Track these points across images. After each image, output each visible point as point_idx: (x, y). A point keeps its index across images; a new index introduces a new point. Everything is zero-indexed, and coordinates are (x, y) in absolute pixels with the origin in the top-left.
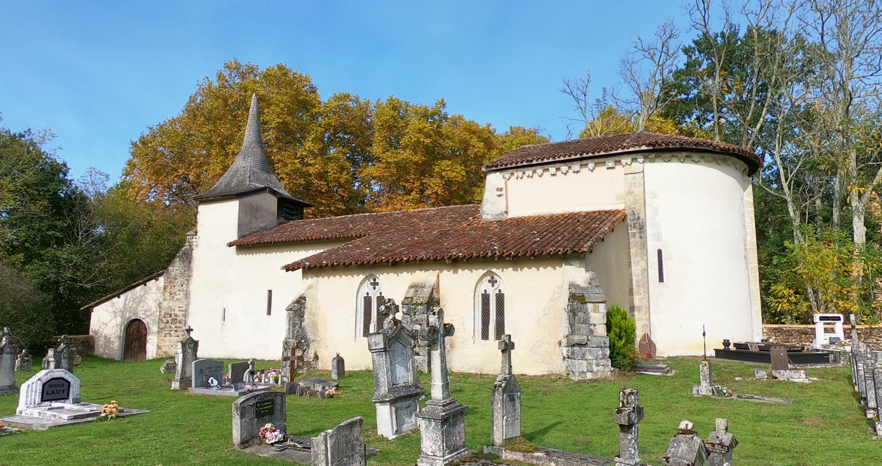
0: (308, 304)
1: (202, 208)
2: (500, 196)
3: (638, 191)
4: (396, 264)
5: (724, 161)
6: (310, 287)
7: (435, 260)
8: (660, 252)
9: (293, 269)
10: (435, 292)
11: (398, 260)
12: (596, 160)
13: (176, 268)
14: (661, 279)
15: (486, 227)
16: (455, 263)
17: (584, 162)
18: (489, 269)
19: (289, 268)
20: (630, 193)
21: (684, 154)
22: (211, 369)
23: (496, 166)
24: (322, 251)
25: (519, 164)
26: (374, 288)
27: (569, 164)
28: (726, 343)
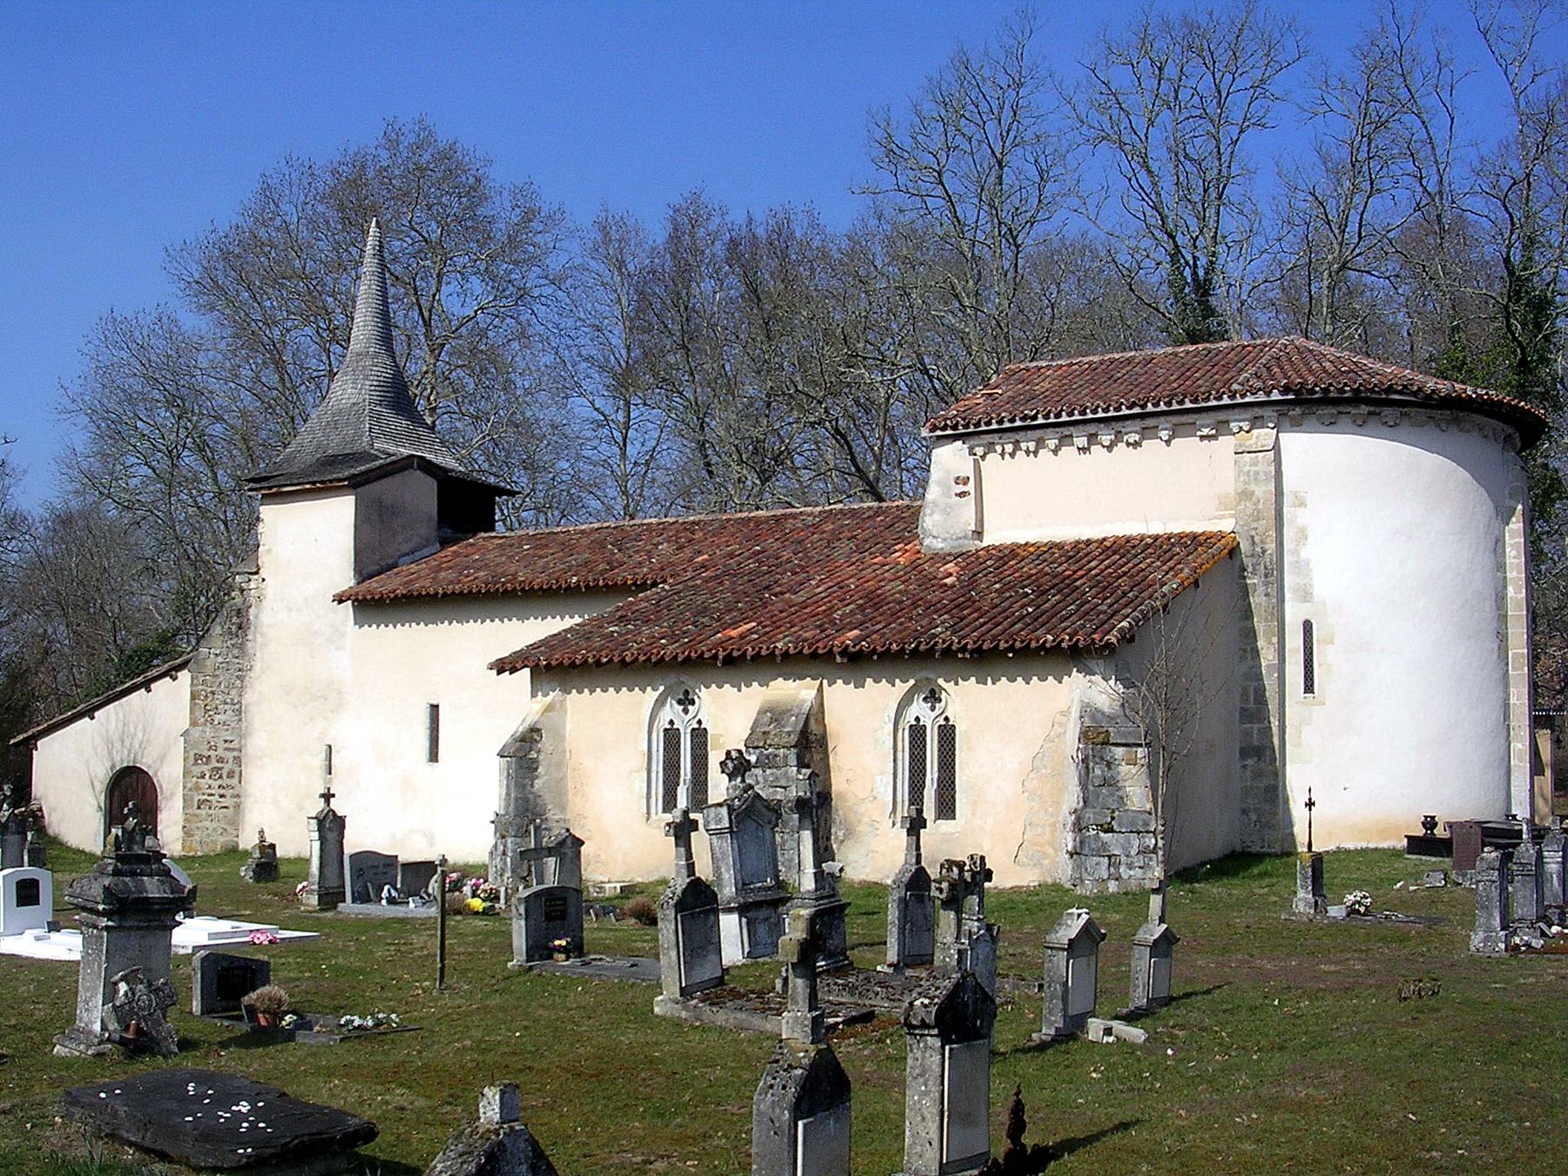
0: (546, 743)
1: (266, 511)
2: (962, 495)
3: (1264, 490)
4: (738, 664)
5: (1457, 421)
6: (549, 708)
7: (814, 656)
8: (1308, 627)
9: (513, 670)
10: (812, 721)
11: (735, 654)
12: (1175, 419)
13: (214, 650)
14: (1309, 688)
15: (922, 571)
16: (858, 663)
17: (1150, 422)
18: (923, 674)
19: (504, 666)
20: (1245, 495)
21: (1364, 409)
22: (376, 871)
23: (955, 427)
24: (568, 622)
25: (1007, 425)
26: (686, 711)
27: (1118, 426)
28: (1430, 823)
